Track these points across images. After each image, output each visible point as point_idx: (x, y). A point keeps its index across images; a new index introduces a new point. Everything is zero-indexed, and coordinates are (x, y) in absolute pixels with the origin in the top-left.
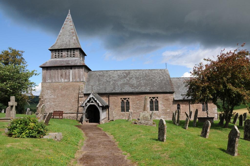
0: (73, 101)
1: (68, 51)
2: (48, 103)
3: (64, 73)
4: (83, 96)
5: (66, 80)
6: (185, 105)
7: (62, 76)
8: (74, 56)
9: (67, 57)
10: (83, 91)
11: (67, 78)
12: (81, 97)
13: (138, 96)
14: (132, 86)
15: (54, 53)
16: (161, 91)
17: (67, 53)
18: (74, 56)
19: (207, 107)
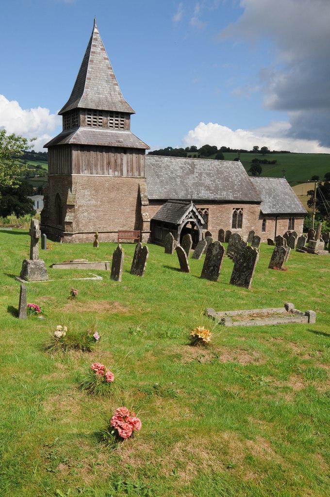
0: (128, 210)
1: (101, 114)
2: (86, 214)
3: (112, 160)
4: (148, 203)
5: (116, 173)
6: (271, 221)
7: (109, 164)
8: (123, 128)
9: (110, 126)
10: (146, 194)
11: (118, 168)
12: (144, 205)
13: (219, 206)
14: (208, 188)
15: (109, 118)
16: (247, 199)
17: (110, 120)
18: (123, 128)
19: (293, 224)
